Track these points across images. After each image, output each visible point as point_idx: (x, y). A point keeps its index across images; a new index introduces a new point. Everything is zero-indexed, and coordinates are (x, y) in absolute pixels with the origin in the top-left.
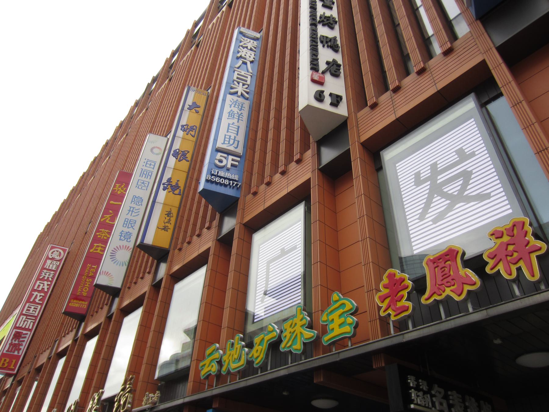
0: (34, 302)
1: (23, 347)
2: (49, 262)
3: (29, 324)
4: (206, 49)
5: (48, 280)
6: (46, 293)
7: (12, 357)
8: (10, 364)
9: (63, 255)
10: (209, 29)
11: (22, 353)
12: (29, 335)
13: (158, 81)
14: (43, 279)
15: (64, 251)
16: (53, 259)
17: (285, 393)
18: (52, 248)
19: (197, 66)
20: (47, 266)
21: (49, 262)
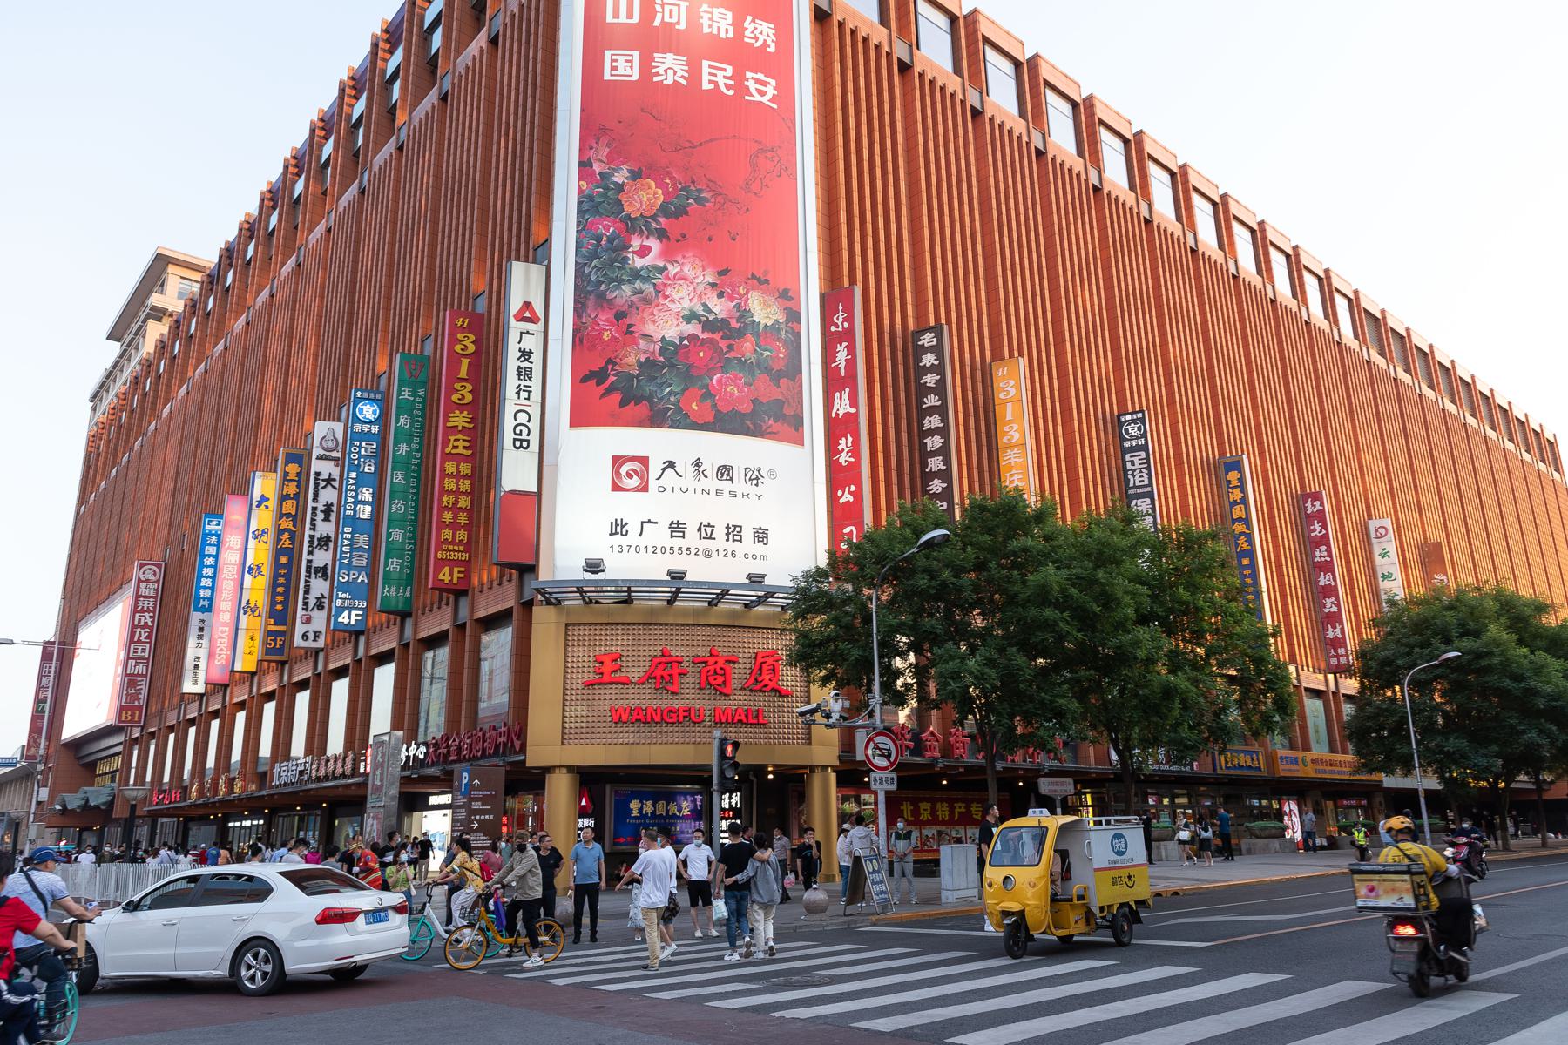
0: (139, 641)
1: (143, 696)
2: (143, 586)
3: (142, 668)
4: (509, 86)
5: (148, 611)
6: (151, 628)
7: (133, 709)
8: (133, 715)
9: (160, 574)
10: (722, 958)
11: (143, 702)
12: (145, 682)
13: (409, 42)
14: (142, 611)
15: (159, 566)
16: (147, 581)
17: (694, 406)
18: (142, 565)
19: (1026, 314)
20: (142, 592)
21: (143, 586)
